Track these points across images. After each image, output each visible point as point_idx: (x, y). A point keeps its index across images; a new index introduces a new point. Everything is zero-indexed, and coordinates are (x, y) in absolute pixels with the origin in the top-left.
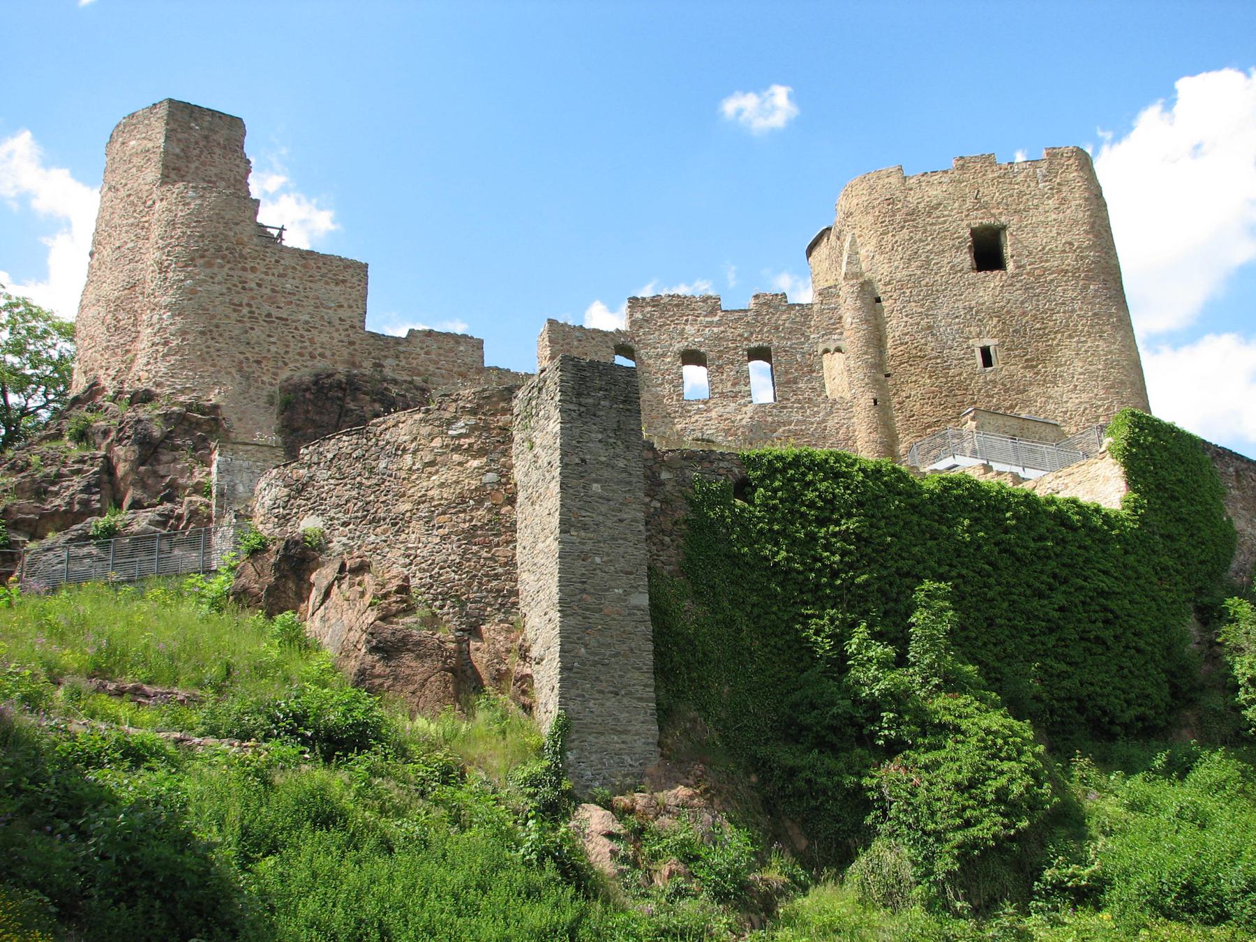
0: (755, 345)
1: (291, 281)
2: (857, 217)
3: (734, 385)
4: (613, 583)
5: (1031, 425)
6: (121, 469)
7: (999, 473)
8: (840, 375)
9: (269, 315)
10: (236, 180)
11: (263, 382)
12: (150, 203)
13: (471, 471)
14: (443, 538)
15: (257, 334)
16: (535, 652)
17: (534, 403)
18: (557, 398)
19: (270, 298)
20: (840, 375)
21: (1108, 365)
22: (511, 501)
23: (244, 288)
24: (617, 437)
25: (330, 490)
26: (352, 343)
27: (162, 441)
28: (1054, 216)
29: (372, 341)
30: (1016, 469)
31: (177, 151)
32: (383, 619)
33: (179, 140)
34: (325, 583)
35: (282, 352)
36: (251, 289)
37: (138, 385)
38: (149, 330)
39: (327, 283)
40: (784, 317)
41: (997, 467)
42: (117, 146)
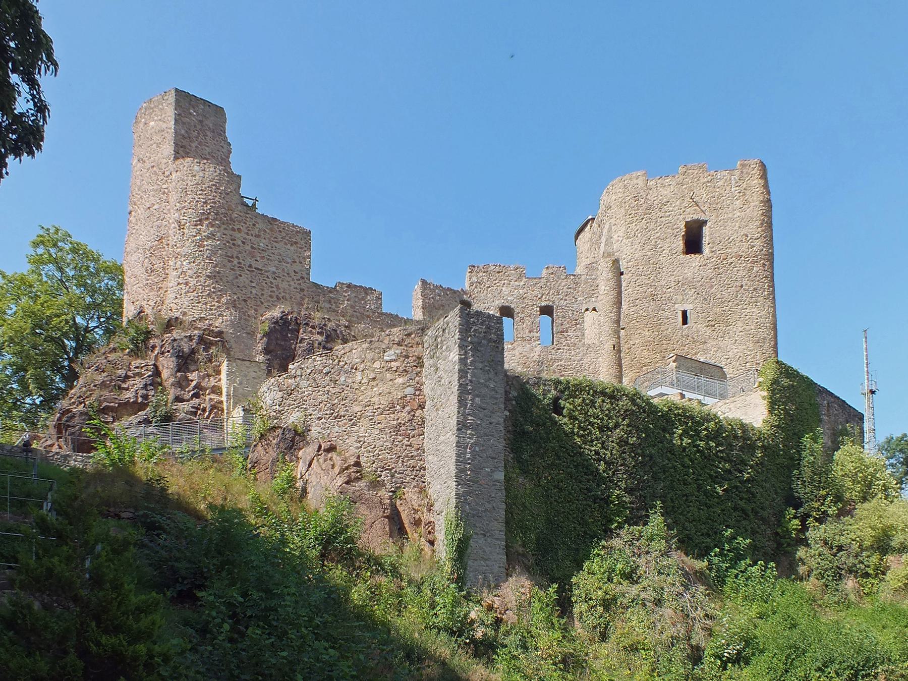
0: (544, 304)
1: (264, 241)
2: (615, 209)
3: (530, 332)
4: (485, 465)
5: (707, 367)
6: (165, 374)
7: (690, 400)
8: (595, 327)
9: (250, 266)
10: (222, 159)
11: (249, 316)
12: (167, 173)
13: (399, 385)
14: (381, 430)
15: (244, 279)
16: (436, 507)
17: (439, 340)
18: (457, 337)
19: (250, 253)
20: (595, 327)
21: (759, 326)
22: (422, 407)
23: (234, 244)
24: (491, 366)
25: (309, 395)
26: (302, 290)
27: (189, 355)
28: (739, 214)
29: (314, 289)
30: (700, 397)
31: (183, 132)
32: (347, 483)
33: (184, 123)
34: (309, 458)
35: (259, 294)
36: (239, 246)
37: (171, 314)
38: (175, 273)
39: (286, 244)
40: (563, 284)
41: (688, 395)
42: (141, 125)
